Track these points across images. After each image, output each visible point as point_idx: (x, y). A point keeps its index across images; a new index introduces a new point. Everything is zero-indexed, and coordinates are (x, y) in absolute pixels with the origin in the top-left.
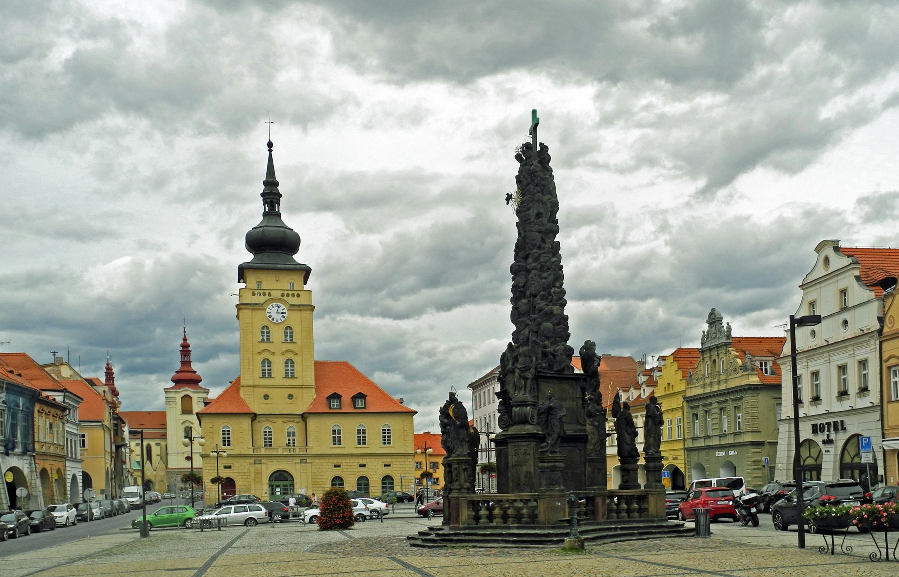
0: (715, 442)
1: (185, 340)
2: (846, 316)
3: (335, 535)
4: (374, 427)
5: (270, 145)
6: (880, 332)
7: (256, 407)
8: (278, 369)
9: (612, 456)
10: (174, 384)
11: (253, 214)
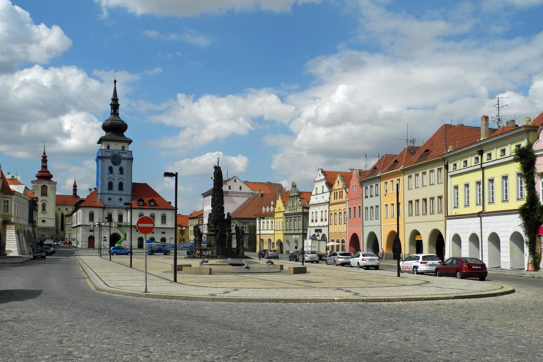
0: (292, 232)
1: (44, 153)
2: (323, 195)
5: (115, 82)
6: (329, 202)
9: (234, 234)
10: (37, 179)
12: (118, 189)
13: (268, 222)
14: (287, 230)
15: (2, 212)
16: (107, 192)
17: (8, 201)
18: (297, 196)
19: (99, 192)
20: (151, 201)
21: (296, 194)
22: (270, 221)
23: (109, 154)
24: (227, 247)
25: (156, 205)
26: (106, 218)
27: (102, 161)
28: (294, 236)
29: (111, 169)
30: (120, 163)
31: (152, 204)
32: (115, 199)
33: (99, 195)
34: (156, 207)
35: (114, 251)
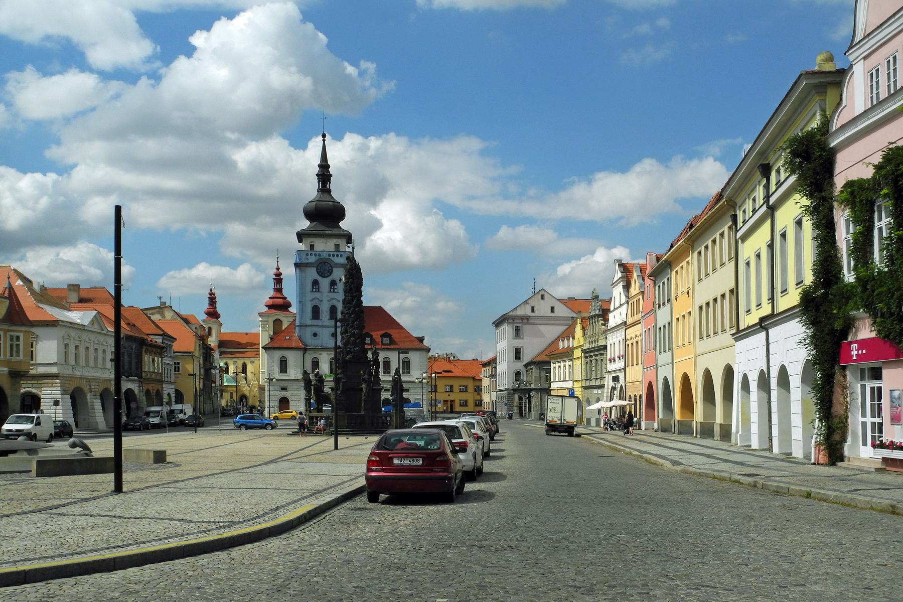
3: (831, 470)
6: (625, 322)
12: (328, 317)
13: (565, 366)
14: (586, 380)
15: (5, 356)
16: (309, 322)
17: (18, 338)
18: (598, 316)
19: (297, 323)
20: (383, 336)
21: (597, 312)
22: (567, 364)
23: (312, 259)
24: (362, 413)
25: (392, 342)
26: (111, 360)
27: (301, 271)
28: (595, 391)
29: (315, 283)
30: (331, 273)
31: (386, 340)
33: (297, 329)
34: (393, 347)
35: (243, 421)
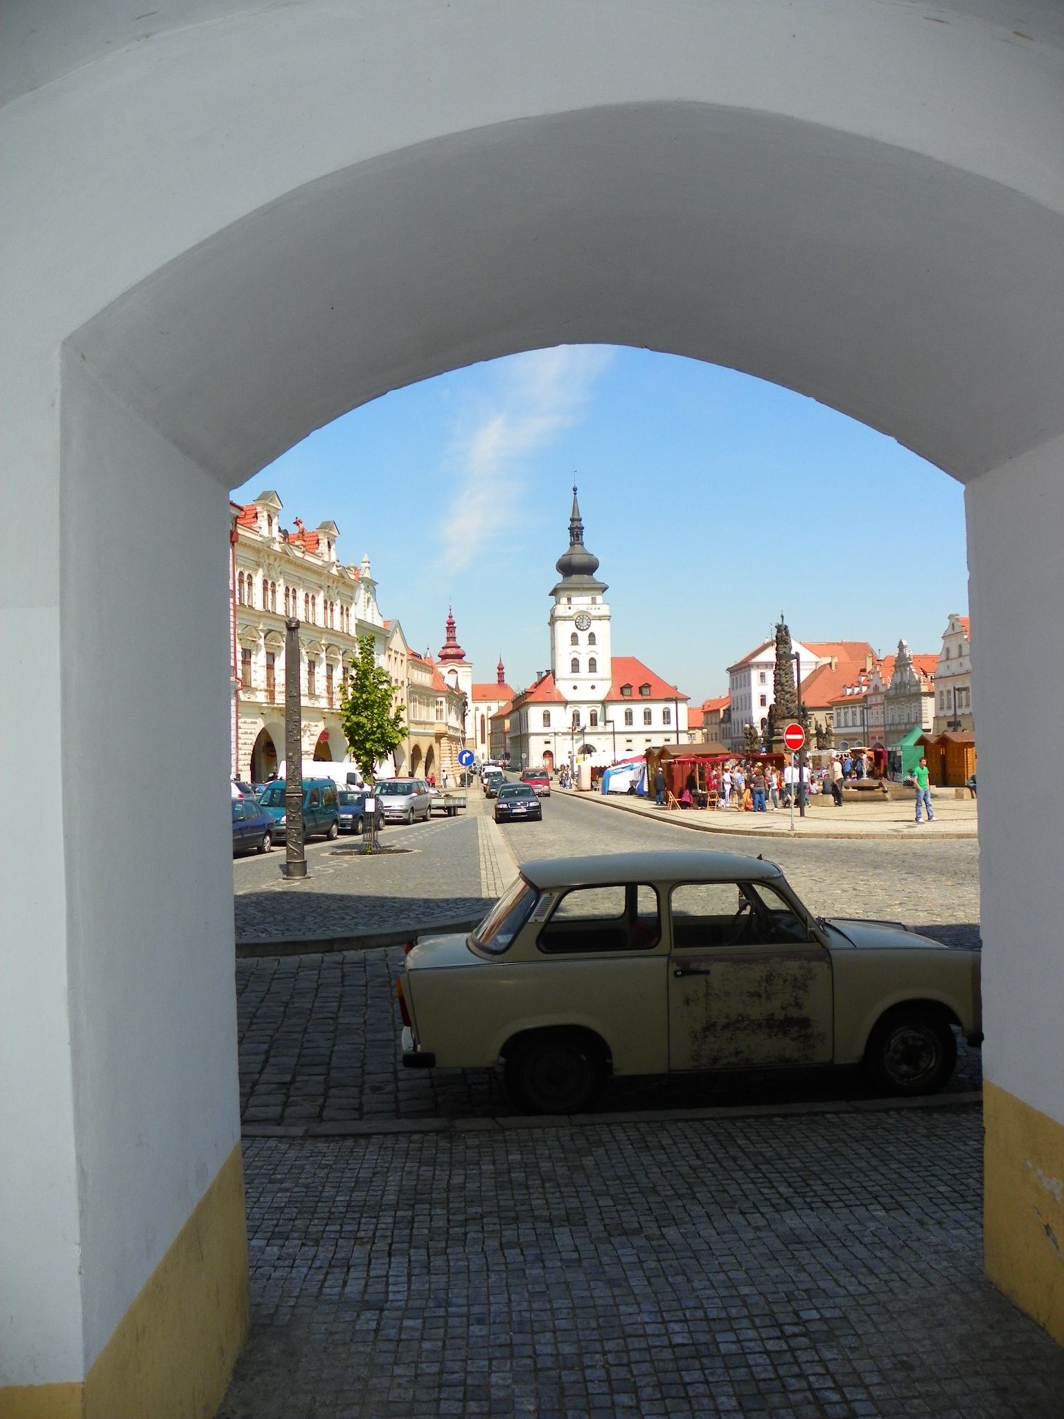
2: (961, 660)
4: (657, 709)
5: (575, 490)
7: (568, 695)
8: (584, 665)
11: (561, 546)
29: (574, 636)
32: (584, 687)
